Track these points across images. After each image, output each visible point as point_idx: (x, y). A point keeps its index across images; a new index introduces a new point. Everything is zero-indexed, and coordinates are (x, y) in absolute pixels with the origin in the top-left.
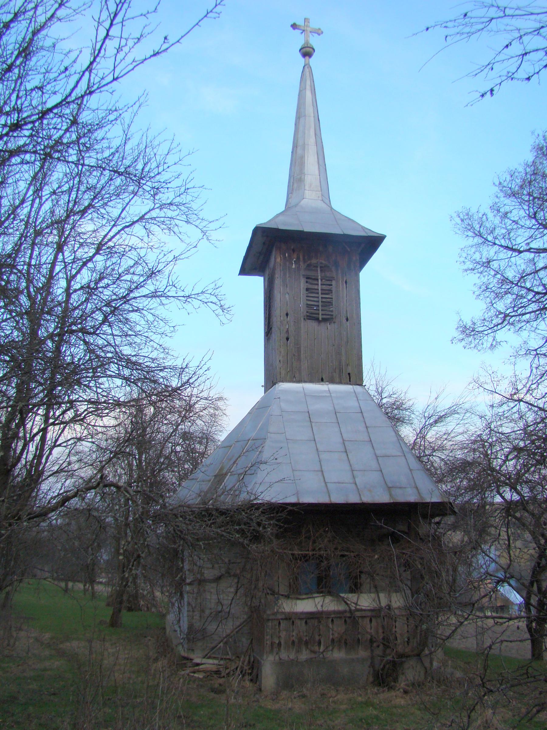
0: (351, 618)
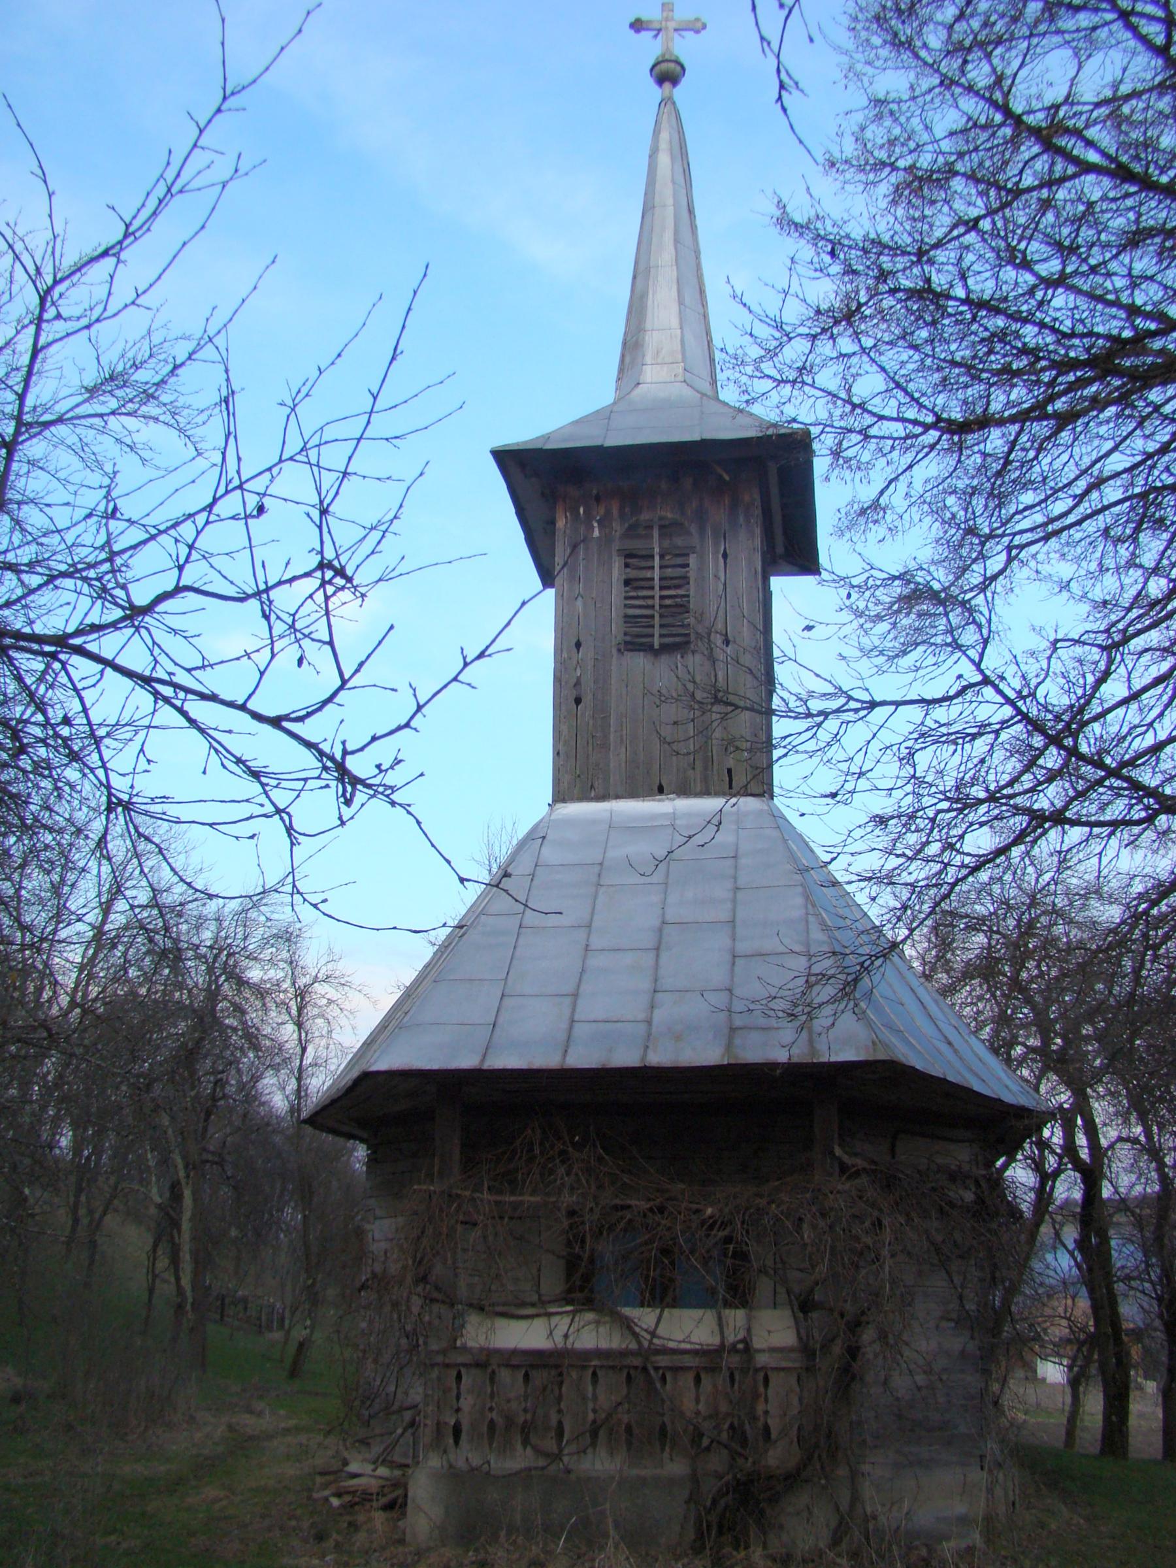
0: (642, 1369)
